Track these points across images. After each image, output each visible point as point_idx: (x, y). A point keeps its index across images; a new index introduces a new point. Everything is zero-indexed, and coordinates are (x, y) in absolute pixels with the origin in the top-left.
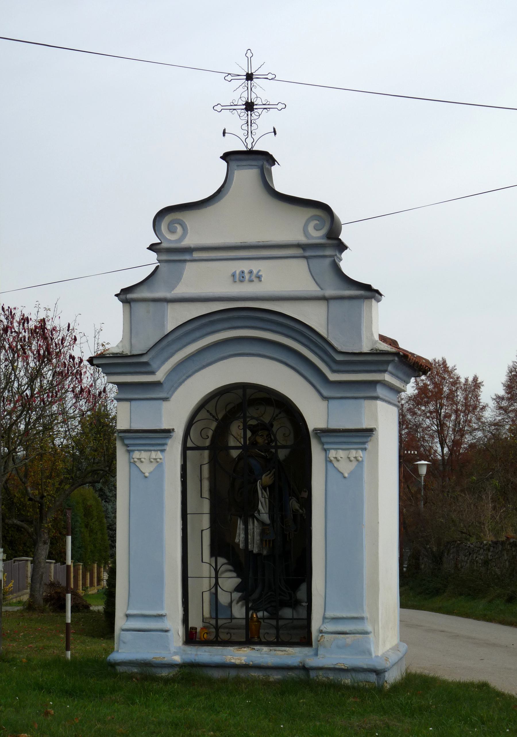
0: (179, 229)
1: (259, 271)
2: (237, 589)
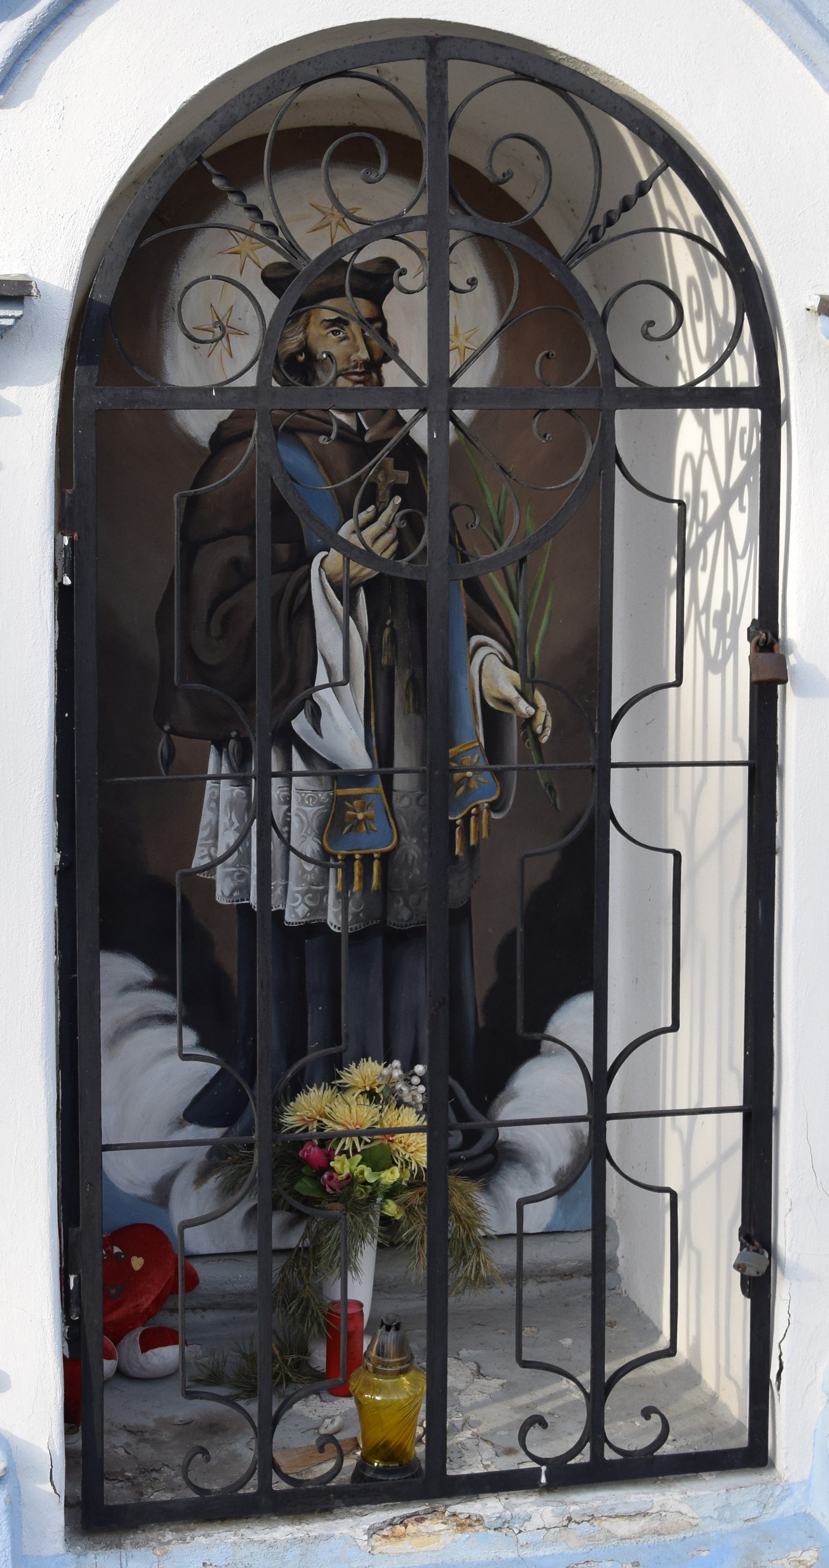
2: (199, 1110)
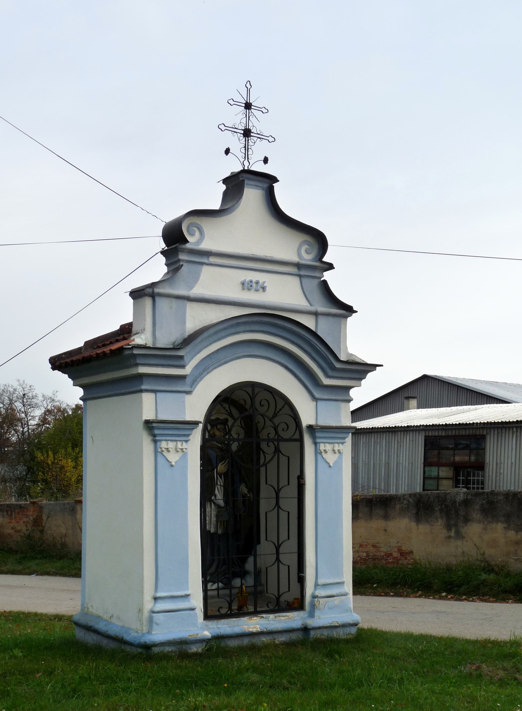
0: (197, 234)
1: (265, 282)
